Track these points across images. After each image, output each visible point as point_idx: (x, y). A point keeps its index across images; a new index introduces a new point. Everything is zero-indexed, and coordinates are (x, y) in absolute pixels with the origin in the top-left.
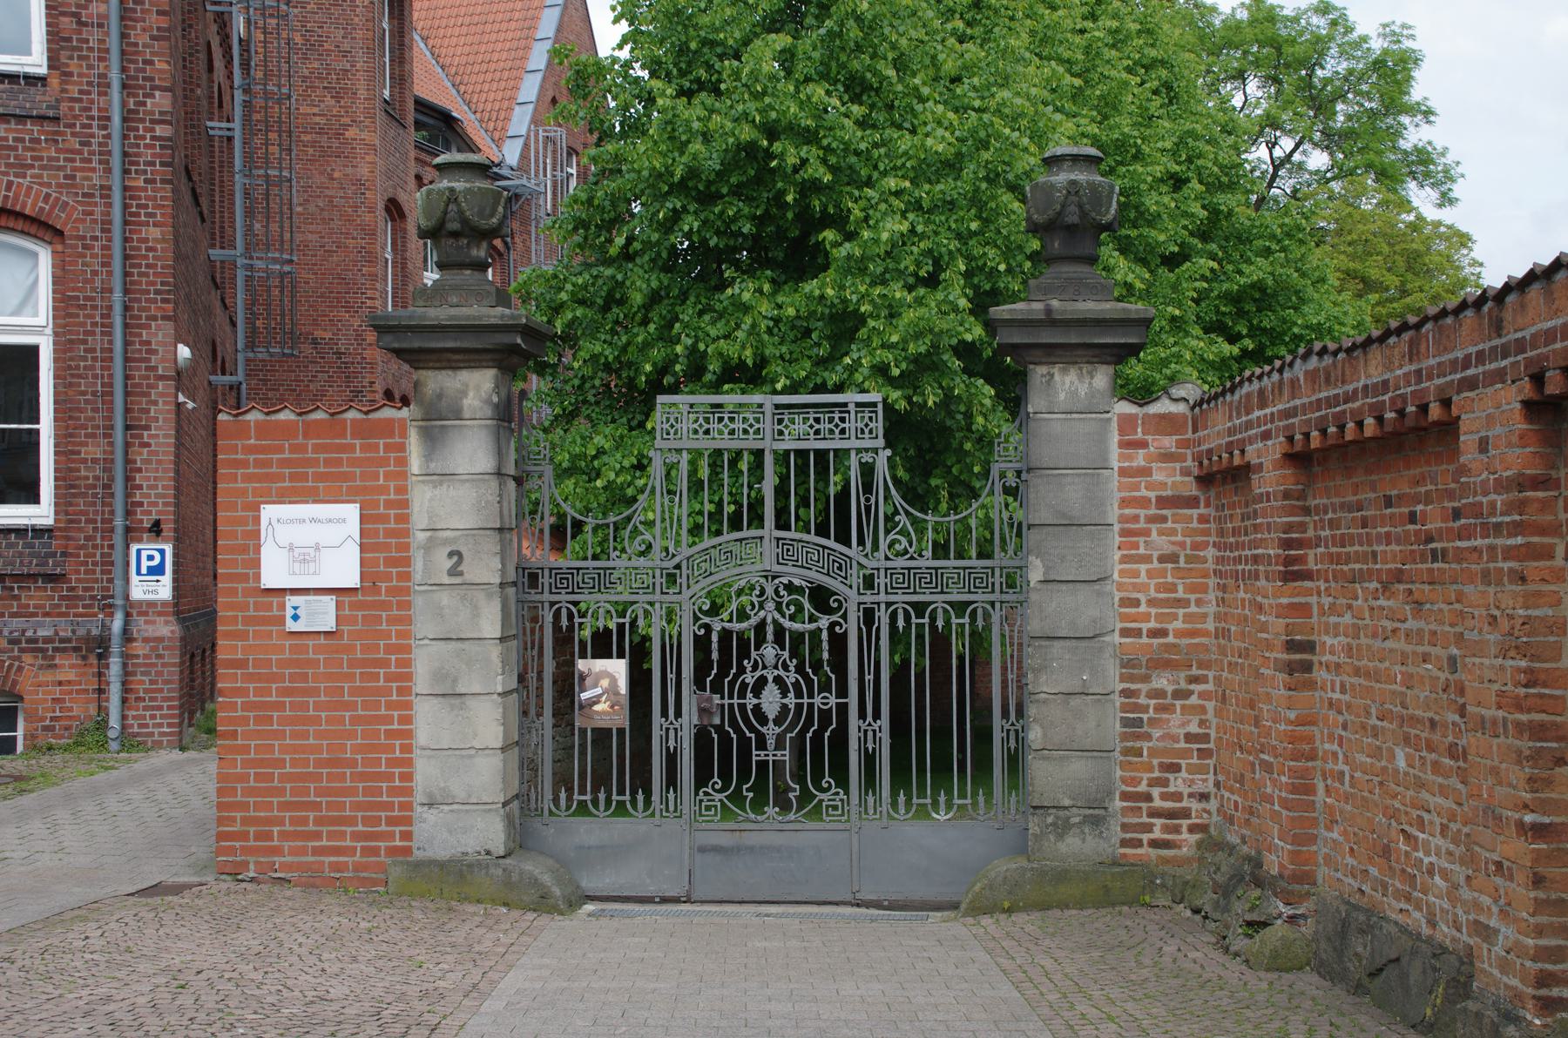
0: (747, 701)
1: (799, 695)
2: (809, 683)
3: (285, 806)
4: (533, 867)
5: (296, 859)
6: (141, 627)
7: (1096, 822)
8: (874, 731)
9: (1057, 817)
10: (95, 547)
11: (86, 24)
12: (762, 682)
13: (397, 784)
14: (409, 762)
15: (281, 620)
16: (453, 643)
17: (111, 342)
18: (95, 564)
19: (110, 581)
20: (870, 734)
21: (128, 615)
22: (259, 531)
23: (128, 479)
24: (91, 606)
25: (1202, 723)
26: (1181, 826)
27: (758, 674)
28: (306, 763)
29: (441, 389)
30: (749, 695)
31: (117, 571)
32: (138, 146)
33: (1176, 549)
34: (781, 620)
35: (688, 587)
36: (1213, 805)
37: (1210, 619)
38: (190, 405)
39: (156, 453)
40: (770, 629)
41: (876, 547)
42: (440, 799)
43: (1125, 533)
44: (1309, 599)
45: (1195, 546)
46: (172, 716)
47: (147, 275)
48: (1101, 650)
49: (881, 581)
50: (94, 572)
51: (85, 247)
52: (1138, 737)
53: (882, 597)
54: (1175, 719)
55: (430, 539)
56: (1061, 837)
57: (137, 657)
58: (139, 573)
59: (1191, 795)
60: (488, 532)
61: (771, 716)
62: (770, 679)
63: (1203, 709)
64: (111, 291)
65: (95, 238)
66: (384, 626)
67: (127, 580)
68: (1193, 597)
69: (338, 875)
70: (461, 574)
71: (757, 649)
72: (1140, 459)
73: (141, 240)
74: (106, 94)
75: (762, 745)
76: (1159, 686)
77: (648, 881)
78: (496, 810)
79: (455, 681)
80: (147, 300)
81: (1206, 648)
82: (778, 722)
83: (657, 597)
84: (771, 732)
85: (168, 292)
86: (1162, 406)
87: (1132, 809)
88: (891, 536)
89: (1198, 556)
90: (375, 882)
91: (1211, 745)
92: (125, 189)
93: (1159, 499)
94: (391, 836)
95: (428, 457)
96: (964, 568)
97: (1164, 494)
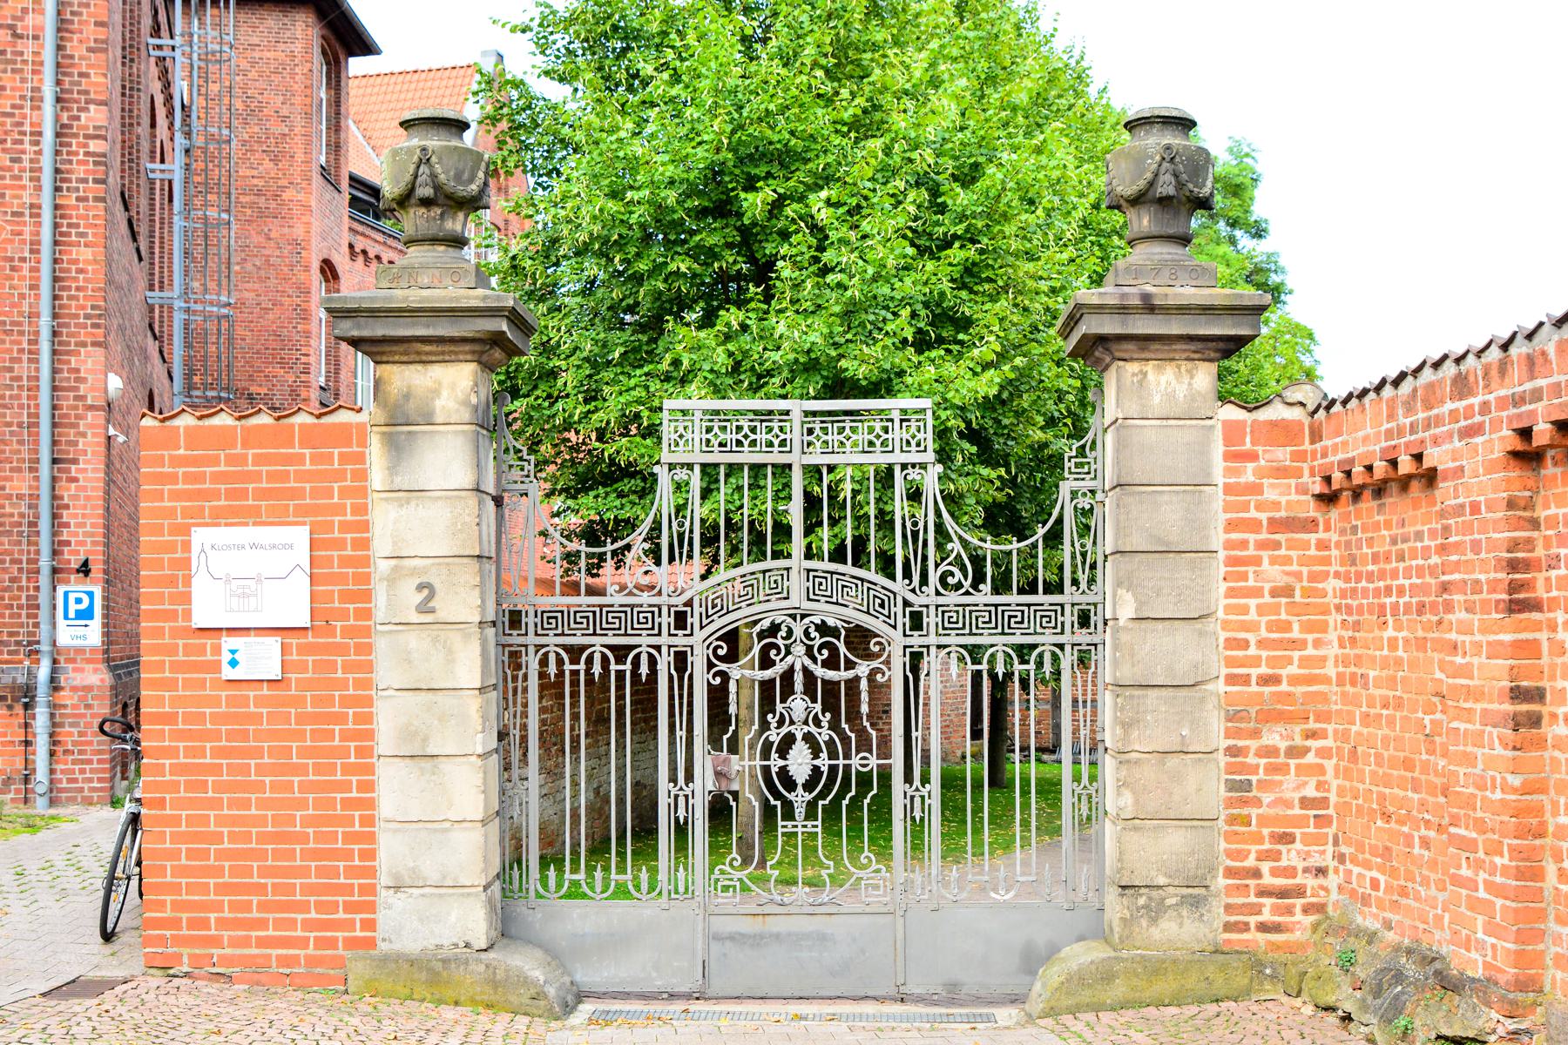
0: (771, 763)
1: (833, 755)
2: (845, 740)
3: (223, 889)
4: (526, 963)
5: (239, 951)
6: (69, 677)
7: (1196, 903)
8: (923, 797)
9: (1150, 899)
10: (20, 589)
11: (21, 37)
12: (789, 740)
13: (357, 863)
14: (371, 838)
15: (216, 667)
16: (423, 694)
17: (37, 370)
18: (20, 607)
19: (37, 625)
20: (917, 801)
21: (55, 661)
22: (189, 559)
23: (54, 516)
24: (16, 652)
25: (1320, 786)
26: (1294, 906)
27: (784, 730)
28: (247, 837)
29: (409, 387)
30: (774, 755)
31: (43, 615)
32: (70, 162)
33: (1290, 580)
34: (812, 667)
35: (702, 628)
36: (1333, 881)
37: (1331, 662)
38: (121, 439)
39: (84, 489)
40: (799, 678)
41: (924, 580)
42: (408, 882)
43: (1232, 561)
44: (1537, 635)
45: (1313, 577)
46: (103, 771)
47: (76, 298)
48: (1202, 700)
49: (930, 620)
50: (19, 616)
51: (13, 269)
52: (1245, 802)
53: (932, 640)
54: (1291, 779)
55: (395, 569)
56: (1154, 921)
57: (65, 706)
58: (66, 617)
59: (1306, 870)
60: (465, 560)
61: (800, 780)
62: (799, 736)
63: (1321, 769)
64: (38, 315)
65: (23, 260)
66: (340, 674)
67: (54, 625)
68: (1310, 637)
69: (288, 971)
70: (432, 611)
71: (783, 701)
72: (1249, 473)
73: (70, 262)
74: (39, 108)
75: (789, 814)
76: (1270, 742)
77: (654, 975)
78: (476, 895)
79: (425, 740)
80: (76, 325)
81: (1324, 698)
82: (809, 786)
83: (664, 640)
84: (800, 799)
85: (100, 316)
86: (1276, 412)
87: (1238, 887)
88: (943, 568)
89: (1316, 589)
90: (331, 980)
91: (1331, 811)
92: (56, 207)
93: (1271, 521)
94: (350, 925)
95: (393, 469)
96: (1029, 605)
97: (1277, 515)
